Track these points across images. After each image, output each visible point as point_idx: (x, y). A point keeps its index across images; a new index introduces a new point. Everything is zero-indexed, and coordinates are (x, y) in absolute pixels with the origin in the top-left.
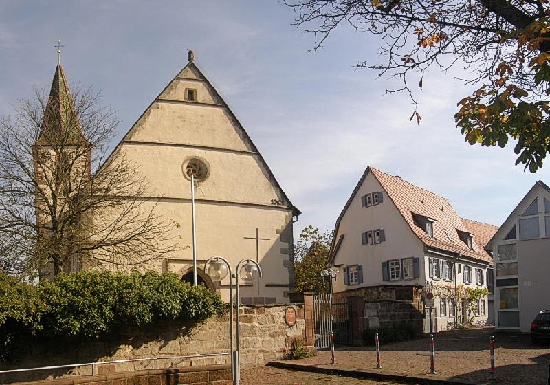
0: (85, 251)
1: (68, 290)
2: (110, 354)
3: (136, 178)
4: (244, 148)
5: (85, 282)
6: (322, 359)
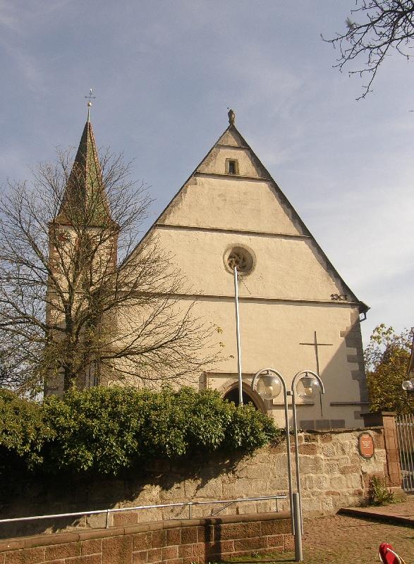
2: (131, 496)
3: (169, 270)
4: (294, 231)
5: (103, 401)
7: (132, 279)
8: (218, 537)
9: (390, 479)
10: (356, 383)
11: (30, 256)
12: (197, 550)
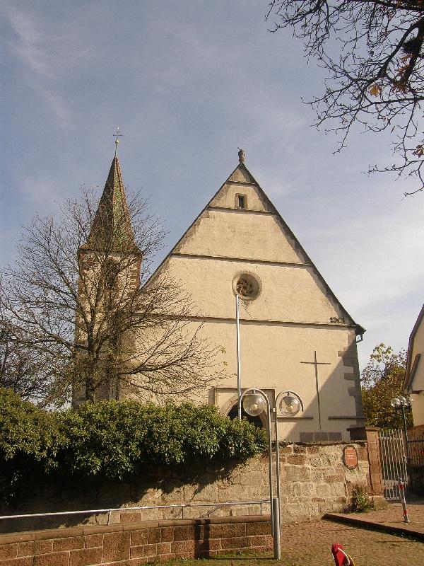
0: (122, 376)
1: (92, 422)
2: (135, 499)
3: (181, 296)
4: (296, 259)
5: (112, 413)
6: (390, 515)
7: (146, 303)
8: (207, 536)
9: (372, 489)
10: (353, 399)
11: (56, 281)
12: (188, 546)
